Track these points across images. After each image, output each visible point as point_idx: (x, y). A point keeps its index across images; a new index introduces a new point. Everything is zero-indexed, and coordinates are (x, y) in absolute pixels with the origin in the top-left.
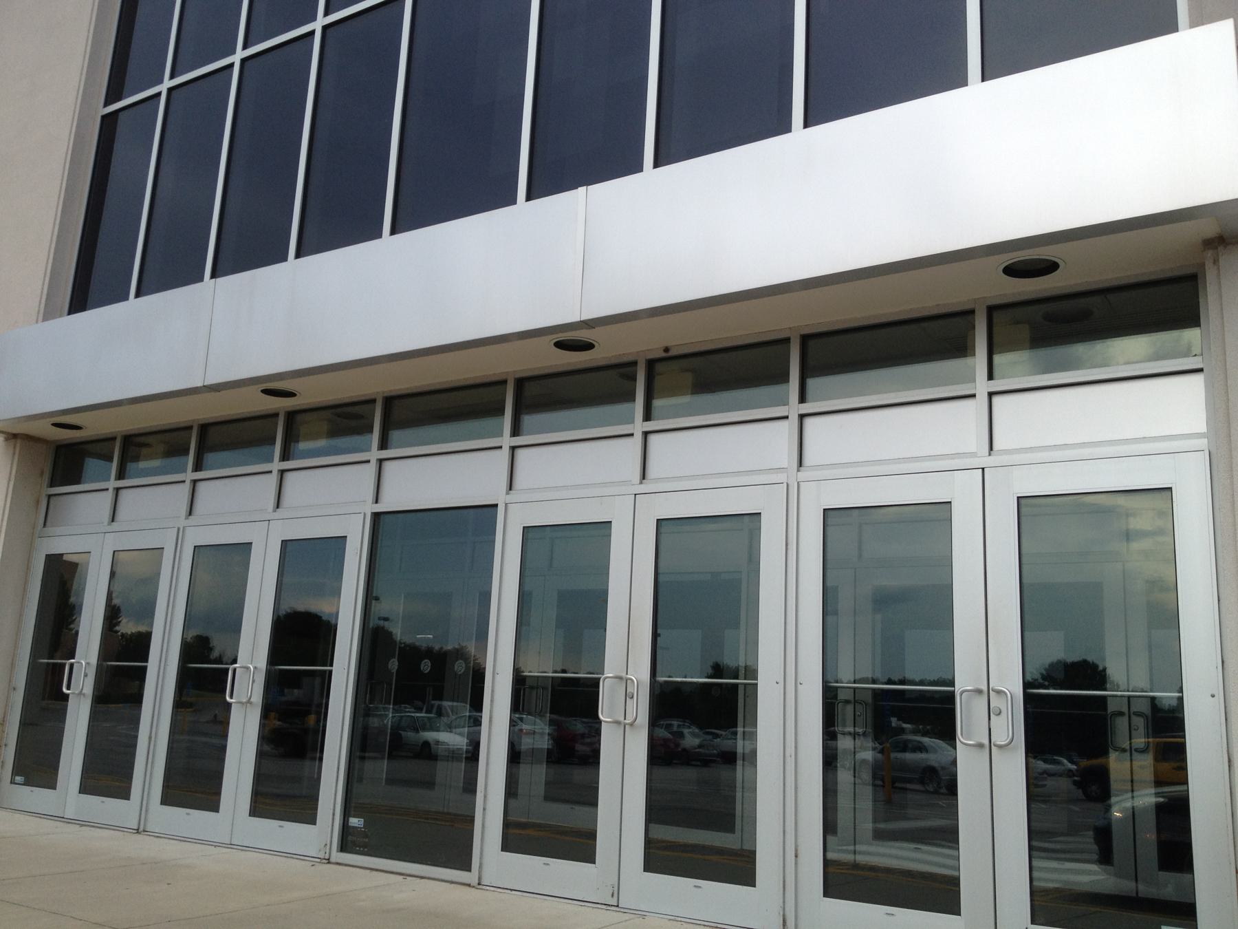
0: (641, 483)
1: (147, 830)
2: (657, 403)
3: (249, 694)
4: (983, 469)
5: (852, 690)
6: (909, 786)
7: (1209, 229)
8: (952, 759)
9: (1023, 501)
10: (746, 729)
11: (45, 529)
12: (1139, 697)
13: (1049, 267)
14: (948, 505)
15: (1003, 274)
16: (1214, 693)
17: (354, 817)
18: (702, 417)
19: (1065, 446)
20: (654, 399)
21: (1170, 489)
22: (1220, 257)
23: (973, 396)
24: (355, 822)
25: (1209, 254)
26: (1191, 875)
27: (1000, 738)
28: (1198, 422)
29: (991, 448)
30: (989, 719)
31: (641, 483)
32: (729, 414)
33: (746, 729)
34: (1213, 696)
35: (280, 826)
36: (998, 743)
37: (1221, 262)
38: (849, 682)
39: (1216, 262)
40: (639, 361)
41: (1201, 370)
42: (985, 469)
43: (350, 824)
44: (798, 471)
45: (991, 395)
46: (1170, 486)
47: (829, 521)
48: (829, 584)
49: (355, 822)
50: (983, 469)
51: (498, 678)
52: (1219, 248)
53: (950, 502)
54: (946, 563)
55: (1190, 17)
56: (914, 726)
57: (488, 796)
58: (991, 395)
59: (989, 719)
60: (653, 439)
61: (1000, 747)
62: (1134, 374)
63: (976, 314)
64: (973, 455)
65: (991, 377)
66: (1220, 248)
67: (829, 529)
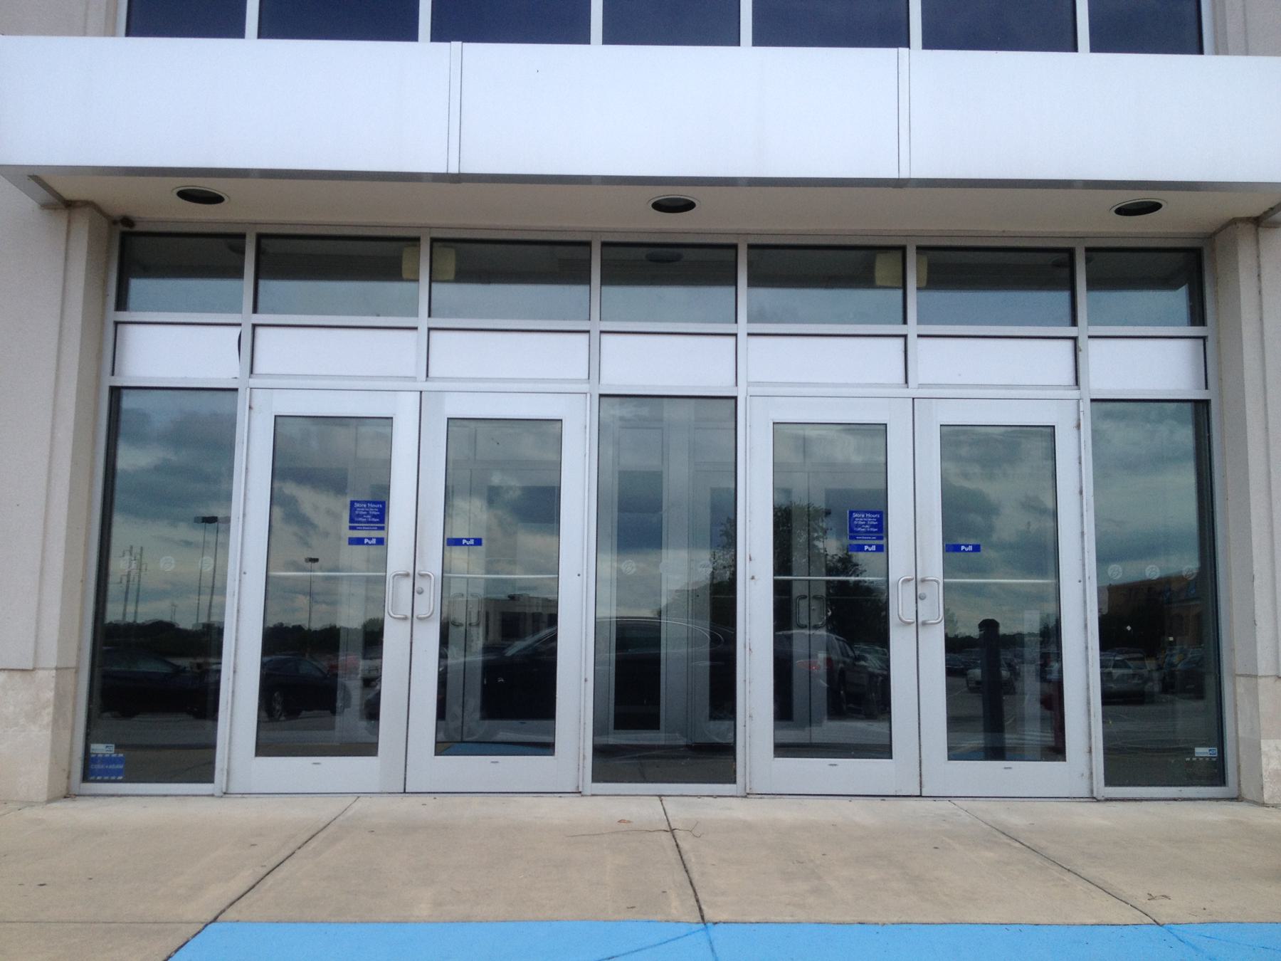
1: (229, 792)
3: (432, 606)
4: (421, 392)
5: (807, 582)
9: (278, 419)
12: (800, 580)
14: (390, 420)
16: (578, 573)
17: (98, 742)
21: (561, 420)
23: (416, 328)
24: (99, 749)
27: (421, 611)
29: (252, 372)
30: (916, 603)
32: (195, 314)
34: (579, 575)
35: (831, 765)
36: (420, 616)
43: (91, 751)
44: (250, 377)
45: (430, 329)
46: (561, 418)
49: (99, 749)
50: (421, 392)
51: (246, 578)
55: (53, 35)
57: (1085, 703)
58: (430, 329)
59: (916, 603)
61: (420, 619)
64: (414, 379)
65: (255, 310)
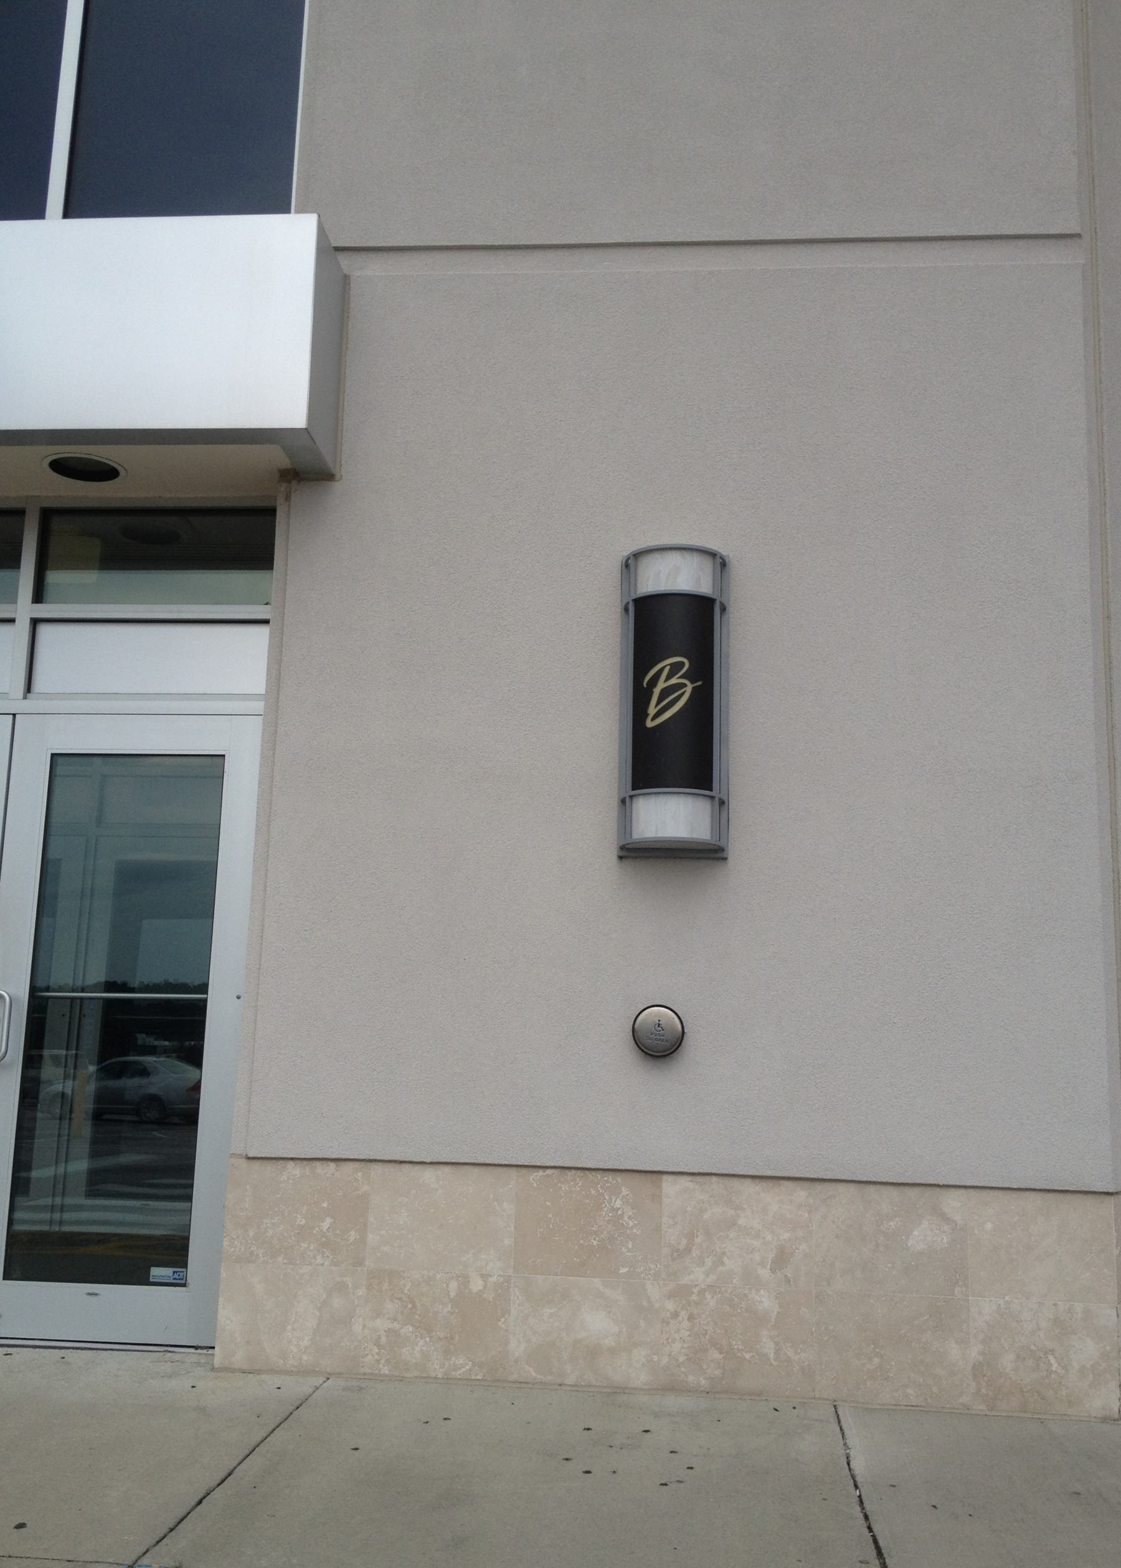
0: (25, 698)
2: (53, 577)
4: (14, 715)
6: (123, 1117)
7: (275, 457)
8: (191, 1084)
10: (64, 1052)
11: (28, 694)
13: (107, 473)
14: (220, 760)
15: (49, 468)
18: (141, 607)
19: (116, 695)
20: (47, 570)
22: (292, 492)
25: (283, 487)
26: (190, 1204)
28: (256, 681)
31: (25, 698)
32: (99, 607)
33: (78, 1052)
34: (238, 997)
37: (293, 499)
38: (95, 988)
39: (288, 498)
40: (27, 510)
41: (266, 622)
42: (17, 715)
47: (59, 770)
48: (51, 855)
52: (293, 482)
53: (224, 756)
54: (211, 833)
56: (175, 1043)
60: (44, 630)
62: (185, 617)
63: (26, 515)
66: (294, 482)
67: (57, 781)
